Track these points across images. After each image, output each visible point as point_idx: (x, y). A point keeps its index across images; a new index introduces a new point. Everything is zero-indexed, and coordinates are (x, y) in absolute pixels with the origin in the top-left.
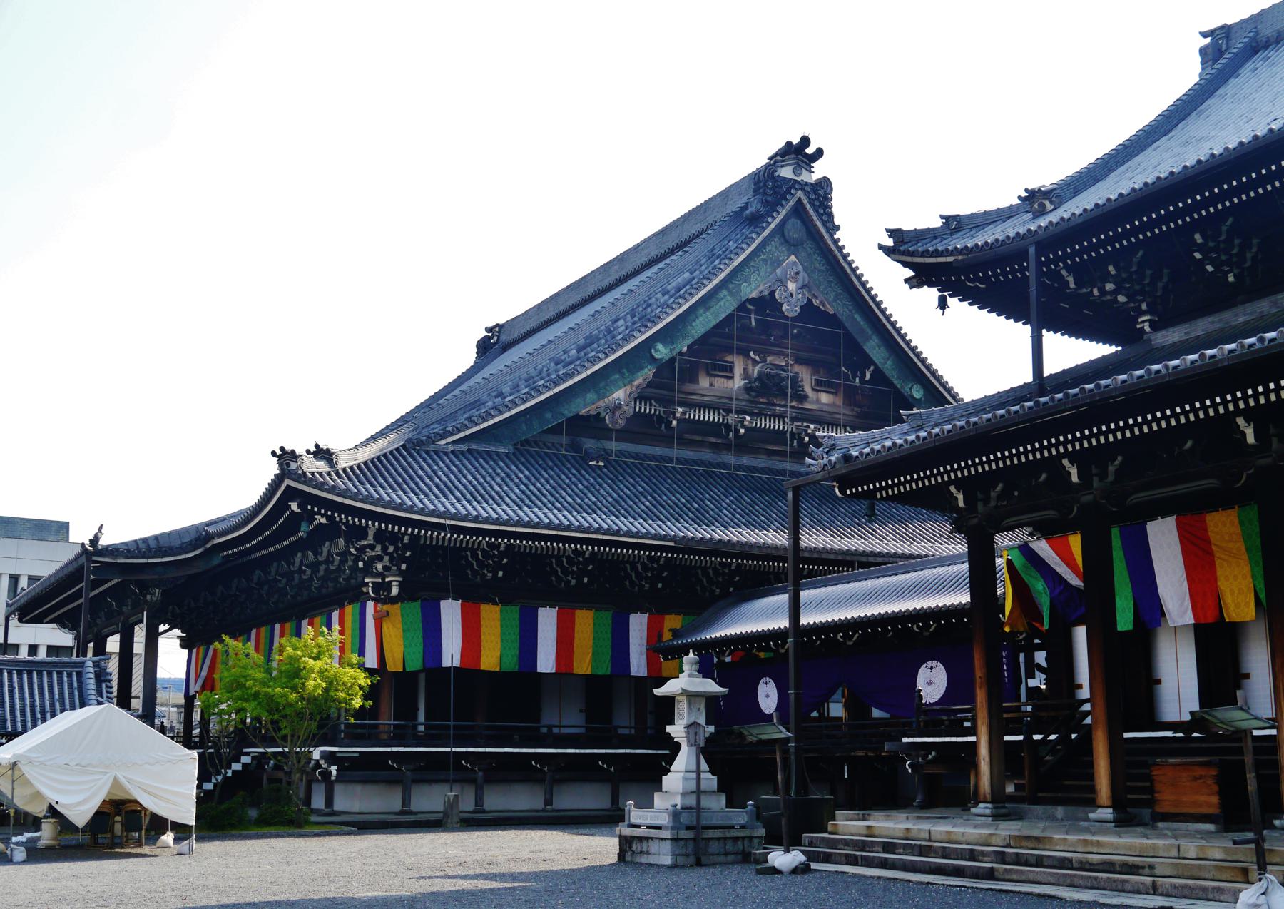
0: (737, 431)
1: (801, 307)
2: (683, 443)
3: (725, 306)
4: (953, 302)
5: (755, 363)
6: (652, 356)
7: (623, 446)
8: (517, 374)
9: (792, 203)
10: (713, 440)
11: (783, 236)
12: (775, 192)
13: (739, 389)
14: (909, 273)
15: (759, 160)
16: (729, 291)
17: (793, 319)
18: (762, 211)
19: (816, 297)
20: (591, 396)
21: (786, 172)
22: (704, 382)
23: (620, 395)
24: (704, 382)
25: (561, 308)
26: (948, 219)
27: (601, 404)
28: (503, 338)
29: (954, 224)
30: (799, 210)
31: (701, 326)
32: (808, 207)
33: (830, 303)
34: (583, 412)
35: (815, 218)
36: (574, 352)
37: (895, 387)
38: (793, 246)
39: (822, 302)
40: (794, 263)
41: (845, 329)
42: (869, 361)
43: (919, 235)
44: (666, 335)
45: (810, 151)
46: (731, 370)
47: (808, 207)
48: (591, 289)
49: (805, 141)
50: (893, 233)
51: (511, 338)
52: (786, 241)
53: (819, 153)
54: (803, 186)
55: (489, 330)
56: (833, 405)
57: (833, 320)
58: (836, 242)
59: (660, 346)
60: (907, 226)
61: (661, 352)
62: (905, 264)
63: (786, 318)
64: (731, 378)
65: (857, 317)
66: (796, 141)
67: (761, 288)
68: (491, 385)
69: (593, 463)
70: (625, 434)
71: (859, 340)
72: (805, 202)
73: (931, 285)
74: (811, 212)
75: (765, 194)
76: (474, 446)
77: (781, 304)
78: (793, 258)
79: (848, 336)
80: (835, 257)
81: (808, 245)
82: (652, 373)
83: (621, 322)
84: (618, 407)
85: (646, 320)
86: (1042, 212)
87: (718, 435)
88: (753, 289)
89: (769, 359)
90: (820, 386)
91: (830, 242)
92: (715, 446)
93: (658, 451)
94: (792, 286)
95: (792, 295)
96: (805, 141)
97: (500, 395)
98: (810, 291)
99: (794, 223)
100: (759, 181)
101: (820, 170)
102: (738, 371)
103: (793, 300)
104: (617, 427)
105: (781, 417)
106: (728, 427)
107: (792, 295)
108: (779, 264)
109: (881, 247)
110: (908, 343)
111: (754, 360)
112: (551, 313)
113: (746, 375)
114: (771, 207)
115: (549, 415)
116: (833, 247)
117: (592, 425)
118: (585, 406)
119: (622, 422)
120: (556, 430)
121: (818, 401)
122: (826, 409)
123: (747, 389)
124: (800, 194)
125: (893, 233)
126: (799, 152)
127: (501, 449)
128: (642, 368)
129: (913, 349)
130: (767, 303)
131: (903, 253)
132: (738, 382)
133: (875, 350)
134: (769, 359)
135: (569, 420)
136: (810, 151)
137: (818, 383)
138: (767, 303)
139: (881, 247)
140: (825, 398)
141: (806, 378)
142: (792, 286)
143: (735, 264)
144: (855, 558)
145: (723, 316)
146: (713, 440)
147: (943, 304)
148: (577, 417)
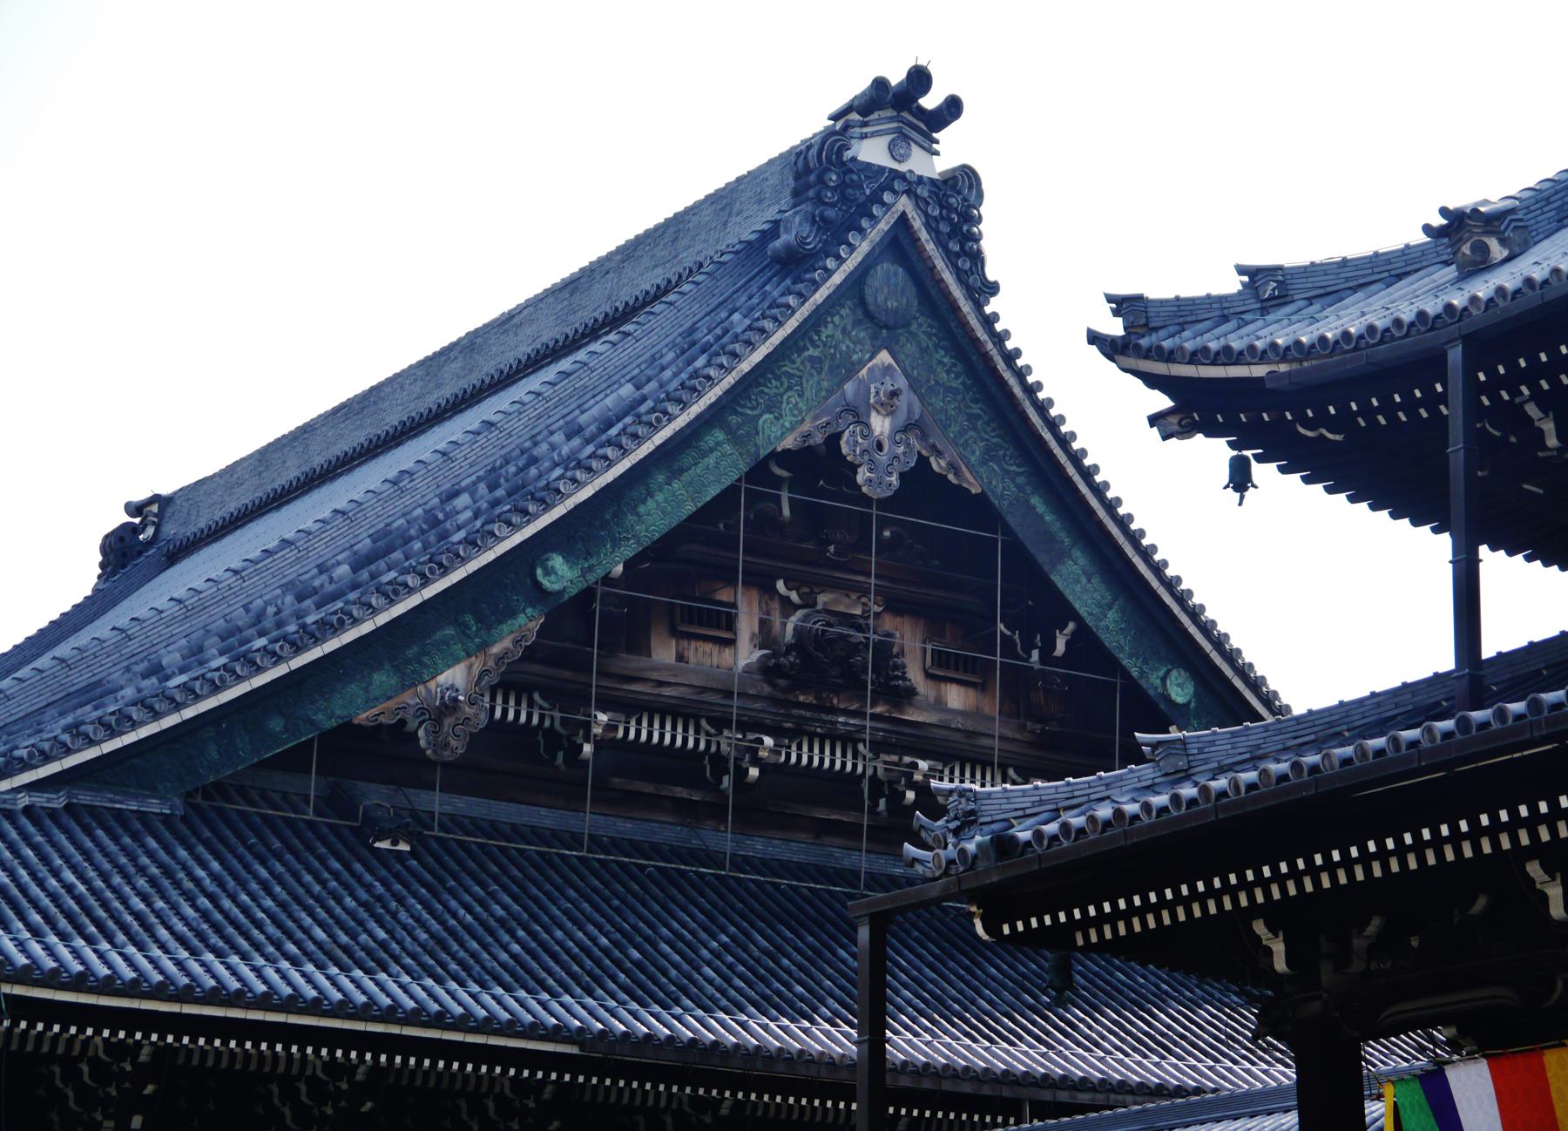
0: (742, 773)
1: (903, 476)
2: (609, 798)
3: (719, 468)
4: (1264, 473)
5: (788, 607)
6: (538, 585)
7: (461, 804)
8: (203, 618)
9: (884, 226)
10: (681, 792)
11: (862, 302)
12: (844, 199)
13: (748, 669)
14: (1161, 401)
15: (807, 120)
16: (729, 431)
17: (884, 504)
18: (812, 243)
19: (939, 454)
20: (382, 679)
21: (872, 151)
22: (664, 652)
23: (455, 677)
24: (664, 652)
25: (318, 461)
26: (1255, 275)
27: (409, 698)
28: (170, 529)
29: (1269, 288)
30: (900, 243)
31: (658, 514)
32: (924, 235)
33: (973, 467)
34: (363, 717)
35: (940, 264)
36: (343, 570)
37: (1126, 673)
38: (884, 329)
39: (952, 466)
40: (887, 370)
41: (1008, 531)
42: (1063, 611)
43: (1185, 312)
44: (571, 535)
45: (930, 101)
46: (730, 623)
47: (924, 235)
48: (393, 418)
49: (920, 79)
50: (1123, 305)
51: (191, 530)
52: (869, 315)
53: (952, 108)
54: (912, 185)
55: (135, 509)
56: (975, 714)
57: (980, 509)
58: (989, 321)
59: (557, 562)
60: (1158, 289)
61: (560, 574)
62: (1152, 381)
63: (866, 500)
64: (731, 643)
65: (1036, 501)
66: (896, 77)
67: (806, 427)
68: (133, 646)
69: (384, 845)
70: (466, 775)
71: (1042, 558)
72: (917, 223)
73: (1212, 431)
74: (930, 247)
75: (819, 200)
76: (85, 798)
77: (854, 468)
78: (884, 357)
79: (1015, 549)
80: (986, 357)
81: (922, 326)
82: (535, 626)
83: (463, 500)
84: (451, 706)
85: (525, 496)
86: (1480, 264)
87: (697, 781)
88: (784, 430)
89: (822, 599)
90: (944, 667)
91: (974, 322)
92: (685, 810)
93: (546, 818)
94: (880, 425)
95: (880, 444)
96: (920, 79)
97: (156, 670)
98: (924, 436)
99: (889, 275)
100: (807, 170)
101: (952, 149)
102: (747, 626)
103: (883, 458)
104: (447, 755)
105: (849, 740)
106: (719, 761)
107: (880, 444)
108: (852, 369)
109: (1094, 338)
110: (1158, 569)
111: (786, 601)
112: (291, 472)
113: (765, 637)
114: (836, 234)
115: (276, 724)
116: (981, 334)
117: (384, 750)
118: (370, 702)
119: (458, 745)
120: (295, 760)
121: (940, 705)
122: (958, 723)
123: (767, 670)
124: (904, 204)
125: (1123, 305)
126: (905, 105)
127: (154, 806)
128: (512, 614)
129: (1171, 584)
130: (821, 464)
131: (1147, 354)
132: (746, 655)
133: (1077, 581)
134: (822, 599)
135: (327, 737)
136: (930, 101)
137: (941, 659)
138: (821, 464)
139: (1094, 338)
140: (956, 697)
141: (912, 649)
142: (880, 425)
143: (745, 366)
144: (1025, 1093)
145: (713, 491)
146: (681, 792)
147: (1240, 480)
148: (348, 729)
